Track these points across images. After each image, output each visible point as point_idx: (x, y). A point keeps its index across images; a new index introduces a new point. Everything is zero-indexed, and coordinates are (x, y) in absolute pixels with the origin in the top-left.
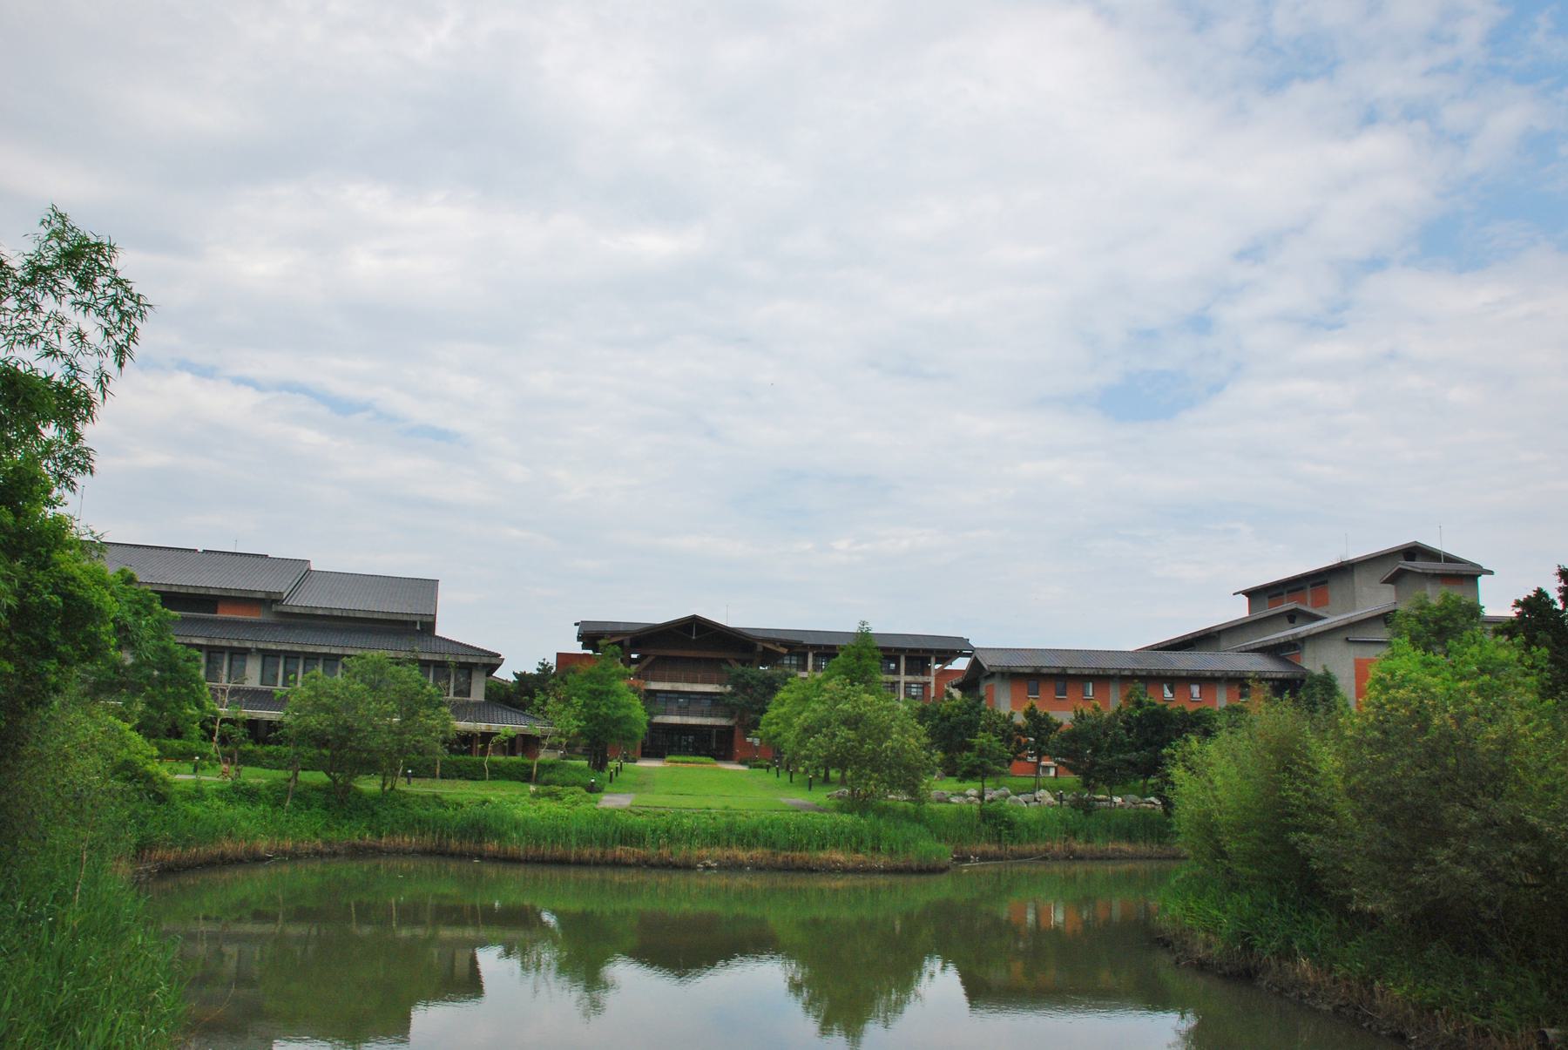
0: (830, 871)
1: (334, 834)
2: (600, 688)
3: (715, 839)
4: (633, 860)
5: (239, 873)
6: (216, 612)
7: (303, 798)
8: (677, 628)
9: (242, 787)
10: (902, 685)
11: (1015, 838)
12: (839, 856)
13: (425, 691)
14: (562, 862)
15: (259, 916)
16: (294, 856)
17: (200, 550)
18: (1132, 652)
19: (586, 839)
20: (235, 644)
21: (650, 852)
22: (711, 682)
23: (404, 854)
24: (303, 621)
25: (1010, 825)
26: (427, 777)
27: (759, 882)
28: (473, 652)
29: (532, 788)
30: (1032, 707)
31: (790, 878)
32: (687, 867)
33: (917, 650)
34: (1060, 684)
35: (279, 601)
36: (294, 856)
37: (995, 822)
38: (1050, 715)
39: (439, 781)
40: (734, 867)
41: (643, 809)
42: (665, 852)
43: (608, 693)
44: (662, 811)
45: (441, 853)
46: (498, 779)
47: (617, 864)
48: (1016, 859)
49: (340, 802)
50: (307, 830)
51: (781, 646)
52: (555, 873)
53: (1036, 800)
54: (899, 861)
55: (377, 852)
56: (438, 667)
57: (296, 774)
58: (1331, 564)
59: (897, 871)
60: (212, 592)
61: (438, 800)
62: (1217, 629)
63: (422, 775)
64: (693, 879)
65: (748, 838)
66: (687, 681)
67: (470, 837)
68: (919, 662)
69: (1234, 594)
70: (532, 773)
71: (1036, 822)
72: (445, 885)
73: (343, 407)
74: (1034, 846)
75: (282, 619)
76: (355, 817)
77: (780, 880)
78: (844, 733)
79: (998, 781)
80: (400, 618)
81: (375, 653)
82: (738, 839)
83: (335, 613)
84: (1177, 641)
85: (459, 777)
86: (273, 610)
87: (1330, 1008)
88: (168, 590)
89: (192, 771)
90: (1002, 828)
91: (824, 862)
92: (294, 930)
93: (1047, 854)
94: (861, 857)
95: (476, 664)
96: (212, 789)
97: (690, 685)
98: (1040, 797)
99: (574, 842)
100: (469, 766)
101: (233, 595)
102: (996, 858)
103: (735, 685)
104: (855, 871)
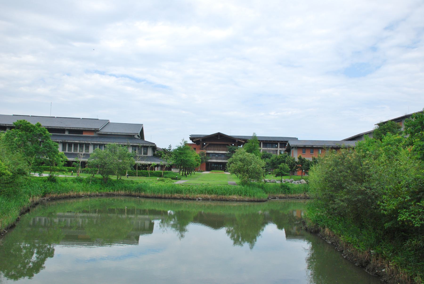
0: (232, 201)
1: (102, 191)
2: (182, 152)
3: (202, 192)
4: (179, 197)
5: (75, 200)
6: (82, 134)
7: (95, 181)
8: (214, 136)
9: (78, 179)
10: (279, 151)
11: (290, 192)
12: (235, 197)
13: (127, 153)
14: (160, 198)
15: (84, 212)
16: (90, 196)
17: (81, 118)
18: (340, 141)
19: (166, 192)
20: (86, 142)
21: (184, 195)
22: (224, 150)
23: (121, 196)
24: (120, 136)
25: (289, 189)
26: (134, 176)
27: (213, 204)
28: (148, 143)
29: (158, 178)
30: (300, 156)
31: (222, 202)
32: (193, 199)
33: (283, 141)
34: (304, 150)
35: (98, 131)
36: (90, 196)
37: (285, 188)
38: (305, 159)
39: (137, 177)
40: (207, 199)
41: (184, 184)
42: (188, 195)
43: (185, 153)
44: (189, 184)
45: (130, 195)
46: (153, 176)
47: (175, 198)
48: (290, 198)
49: (105, 182)
50: (94, 189)
51: (243, 140)
52: (159, 201)
53: (301, 182)
54: (252, 198)
55: (114, 195)
56: (133, 147)
57: (94, 175)
58: (402, 116)
59: (251, 201)
60: (81, 129)
61: (132, 182)
62: (361, 134)
63: (133, 175)
64: (195, 202)
65: (210, 192)
66: (217, 150)
67: (137, 191)
68: (284, 145)
69: (375, 125)
70: (162, 175)
71: (296, 188)
72: (131, 204)
73: (138, 81)
74: (295, 195)
75: (100, 136)
76: (109, 186)
77: (219, 203)
78: (239, 163)
79: (291, 177)
80: (130, 134)
81: (113, 144)
82: (207, 192)
83: (113, 133)
84: (351, 138)
85: (143, 176)
86: (97, 133)
87: (331, 243)
88: (70, 129)
89: (71, 175)
90: (286, 190)
91: (231, 199)
92: (95, 215)
93: (299, 197)
94: (241, 197)
95: (148, 146)
96: (70, 179)
97: (218, 151)
98: (302, 181)
99: (163, 192)
100: (145, 173)
101: (86, 129)
102: (284, 198)
103: (230, 151)
104: (240, 201)
